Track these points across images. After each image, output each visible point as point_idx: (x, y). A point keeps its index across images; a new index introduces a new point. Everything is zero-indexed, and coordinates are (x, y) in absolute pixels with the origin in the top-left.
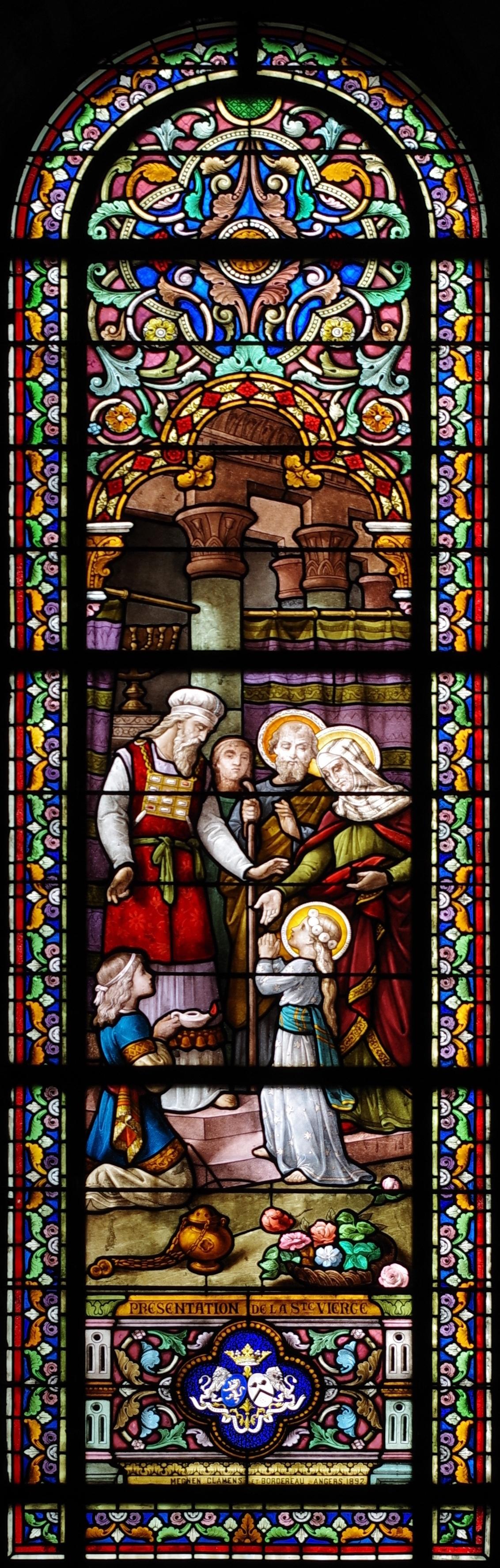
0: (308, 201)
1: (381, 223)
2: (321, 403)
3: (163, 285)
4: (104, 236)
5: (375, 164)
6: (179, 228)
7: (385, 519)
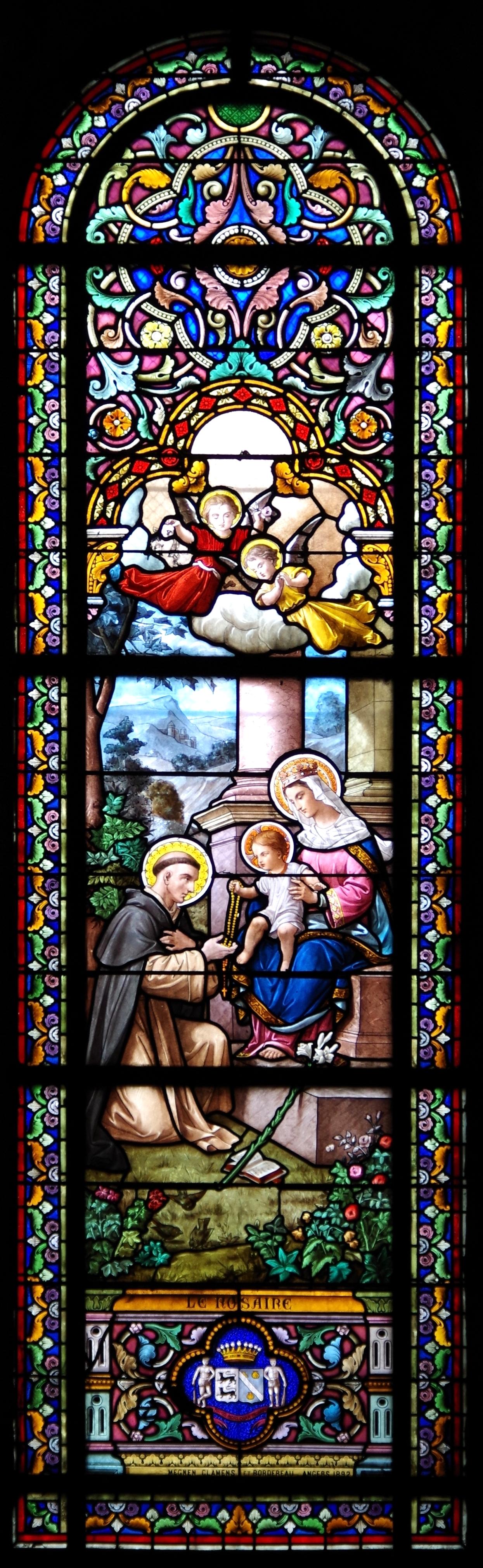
0: (294, 207)
1: (368, 228)
2: (310, 409)
4: (102, 241)
5: (359, 172)
6: (173, 234)
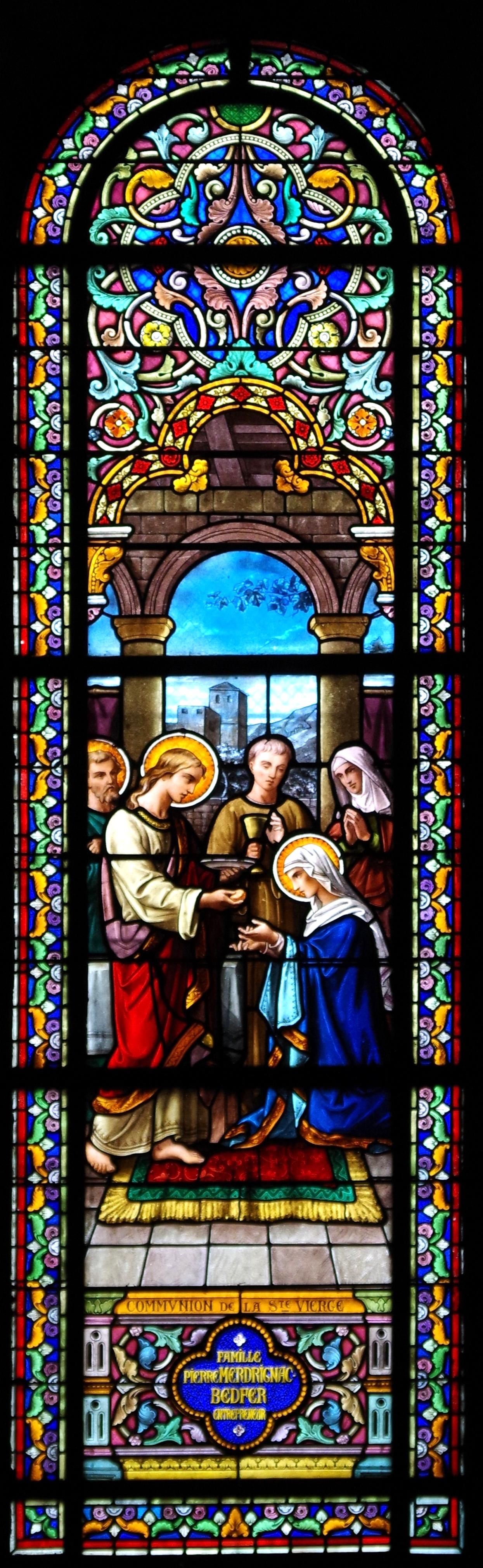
0: (295, 206)
1: (365, 229)
2: (309, 407)
3: (159, 289)
4: (105, 241)
6: (177, 234)
7: (370, 524)
